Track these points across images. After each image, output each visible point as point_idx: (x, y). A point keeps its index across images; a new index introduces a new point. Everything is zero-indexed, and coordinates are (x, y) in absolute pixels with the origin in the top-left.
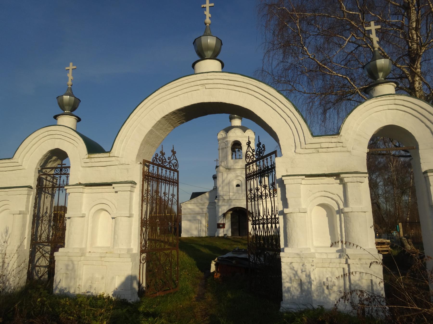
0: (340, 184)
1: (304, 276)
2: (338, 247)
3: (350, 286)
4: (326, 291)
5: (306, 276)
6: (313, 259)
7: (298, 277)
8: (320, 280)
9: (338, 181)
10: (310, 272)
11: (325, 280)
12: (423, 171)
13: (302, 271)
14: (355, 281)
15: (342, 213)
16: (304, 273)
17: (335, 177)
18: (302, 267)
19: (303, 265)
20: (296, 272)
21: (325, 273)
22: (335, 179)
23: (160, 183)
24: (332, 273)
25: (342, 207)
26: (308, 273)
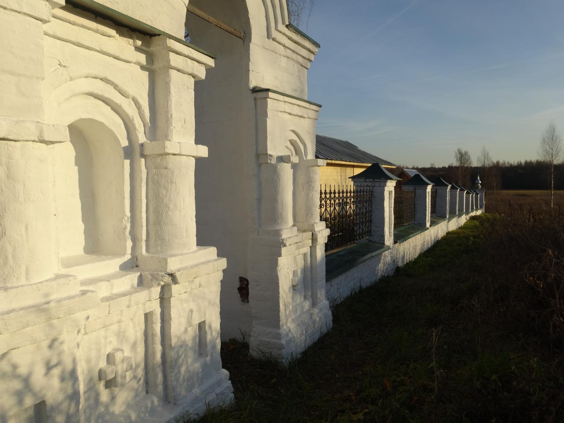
0: (143, 68)
1: (56, 382)
2: (124, 254)
3: (164, 355)
4: (104, 395)
5: (63, 379)
6: (90, 312)
7: (34, 395)
8: (90, 371)
9: (142, 58)
10: (74, 361)
11: (103, 364)
12: (252, 84)
13: (49, 368)
14: (179, 338)
15: (143, 155)
16: (56, 372)
17: (139, 43)
18: (47, 353)
19: (50, 347)
20: (26, 380)
21: (103, 341)
22: (137, 49)
23: (352, 190)
24: (121, 335)
25: (142, 138)
26: (69, 367)
